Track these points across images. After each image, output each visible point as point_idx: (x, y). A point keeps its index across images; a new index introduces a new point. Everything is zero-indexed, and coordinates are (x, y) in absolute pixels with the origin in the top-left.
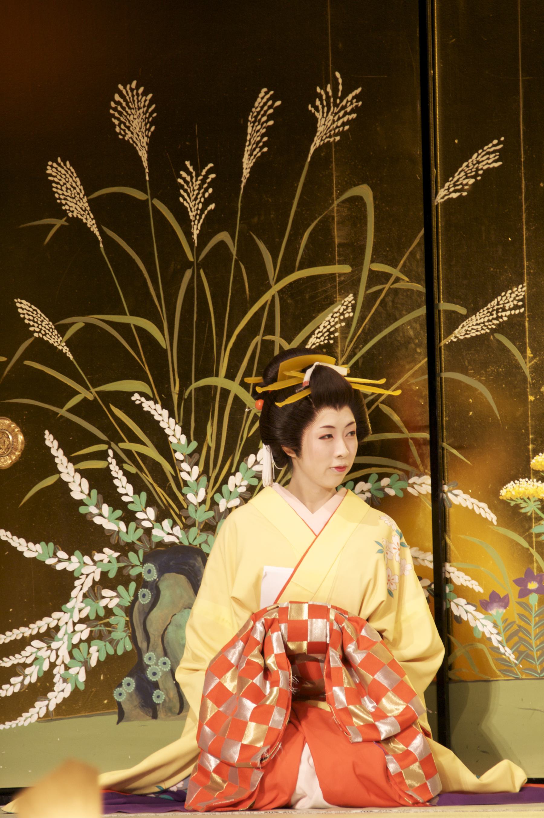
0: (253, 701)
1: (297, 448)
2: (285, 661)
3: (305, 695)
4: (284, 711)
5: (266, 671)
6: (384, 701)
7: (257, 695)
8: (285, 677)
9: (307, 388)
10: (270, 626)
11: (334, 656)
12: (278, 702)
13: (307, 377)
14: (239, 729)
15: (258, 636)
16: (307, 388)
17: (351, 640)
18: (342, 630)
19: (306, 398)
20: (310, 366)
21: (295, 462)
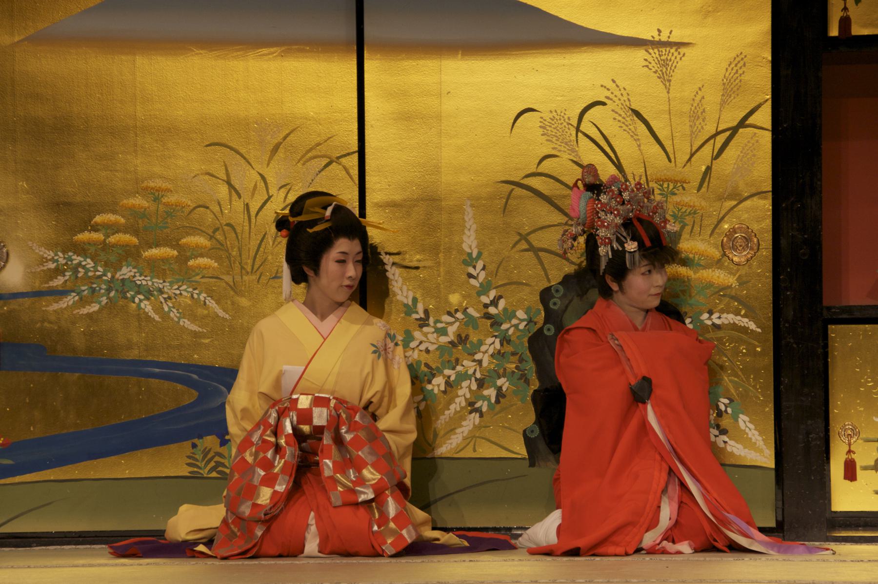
0: (264, 471)
1: (316, 266)
2: (293, 440)
3: (305, 468)
4: (287, 478)
5: (278, 449)
6: (365, 472)
7: (267, 465)
8: (290, 453)
9: (327, 221)
10: (282, 414)
11: (327, 440)
12: (283, 470)
13: (328, 212)
14: (251, 491)
15: (272, 421)
16: (327, 221)
17: (344, 424)
18: (339, 416)
19: (326, 229)
20: (330, 205)
21: (311, 280)
